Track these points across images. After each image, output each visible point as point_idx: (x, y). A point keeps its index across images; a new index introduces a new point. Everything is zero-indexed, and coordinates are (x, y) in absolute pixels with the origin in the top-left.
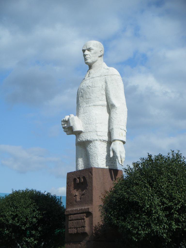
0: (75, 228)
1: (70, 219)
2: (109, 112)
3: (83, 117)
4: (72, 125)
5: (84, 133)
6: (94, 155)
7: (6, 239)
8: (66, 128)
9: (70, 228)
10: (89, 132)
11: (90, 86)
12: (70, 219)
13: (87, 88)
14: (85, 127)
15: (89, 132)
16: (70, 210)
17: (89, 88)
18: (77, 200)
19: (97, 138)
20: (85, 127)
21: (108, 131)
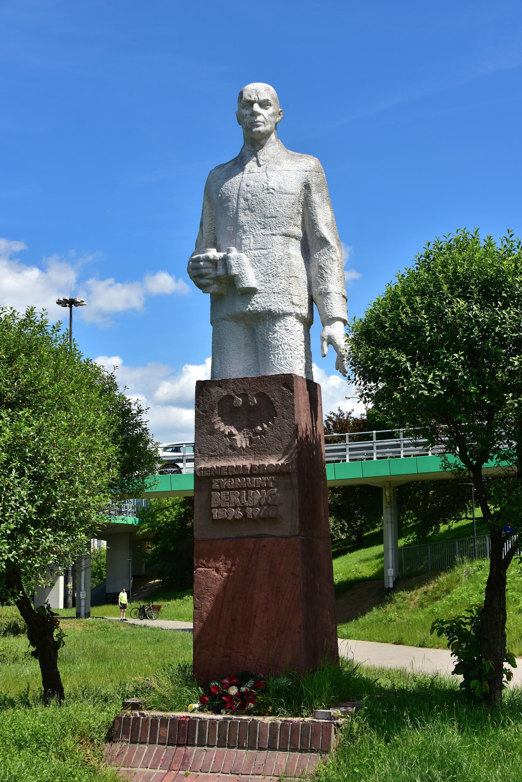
0: (235, 508)
1: (216, 486)
2: (307, 252)
3: (255, 257)
4: (235, 271)
5: (259, 293)
6: (283, 346)
7: (489, 505)
8: (209, 276)
9: (219, 507)
10: (274, 293)
11: (272, 189)
12: (216, 486)
13: (266, 191)
14: (262, 282)
15: (273, 295)
16: (267, 464)
17: (272, 194)
18: (239, 446)
19: (289, 308)
20: (262, 282)
21: (307, 296)
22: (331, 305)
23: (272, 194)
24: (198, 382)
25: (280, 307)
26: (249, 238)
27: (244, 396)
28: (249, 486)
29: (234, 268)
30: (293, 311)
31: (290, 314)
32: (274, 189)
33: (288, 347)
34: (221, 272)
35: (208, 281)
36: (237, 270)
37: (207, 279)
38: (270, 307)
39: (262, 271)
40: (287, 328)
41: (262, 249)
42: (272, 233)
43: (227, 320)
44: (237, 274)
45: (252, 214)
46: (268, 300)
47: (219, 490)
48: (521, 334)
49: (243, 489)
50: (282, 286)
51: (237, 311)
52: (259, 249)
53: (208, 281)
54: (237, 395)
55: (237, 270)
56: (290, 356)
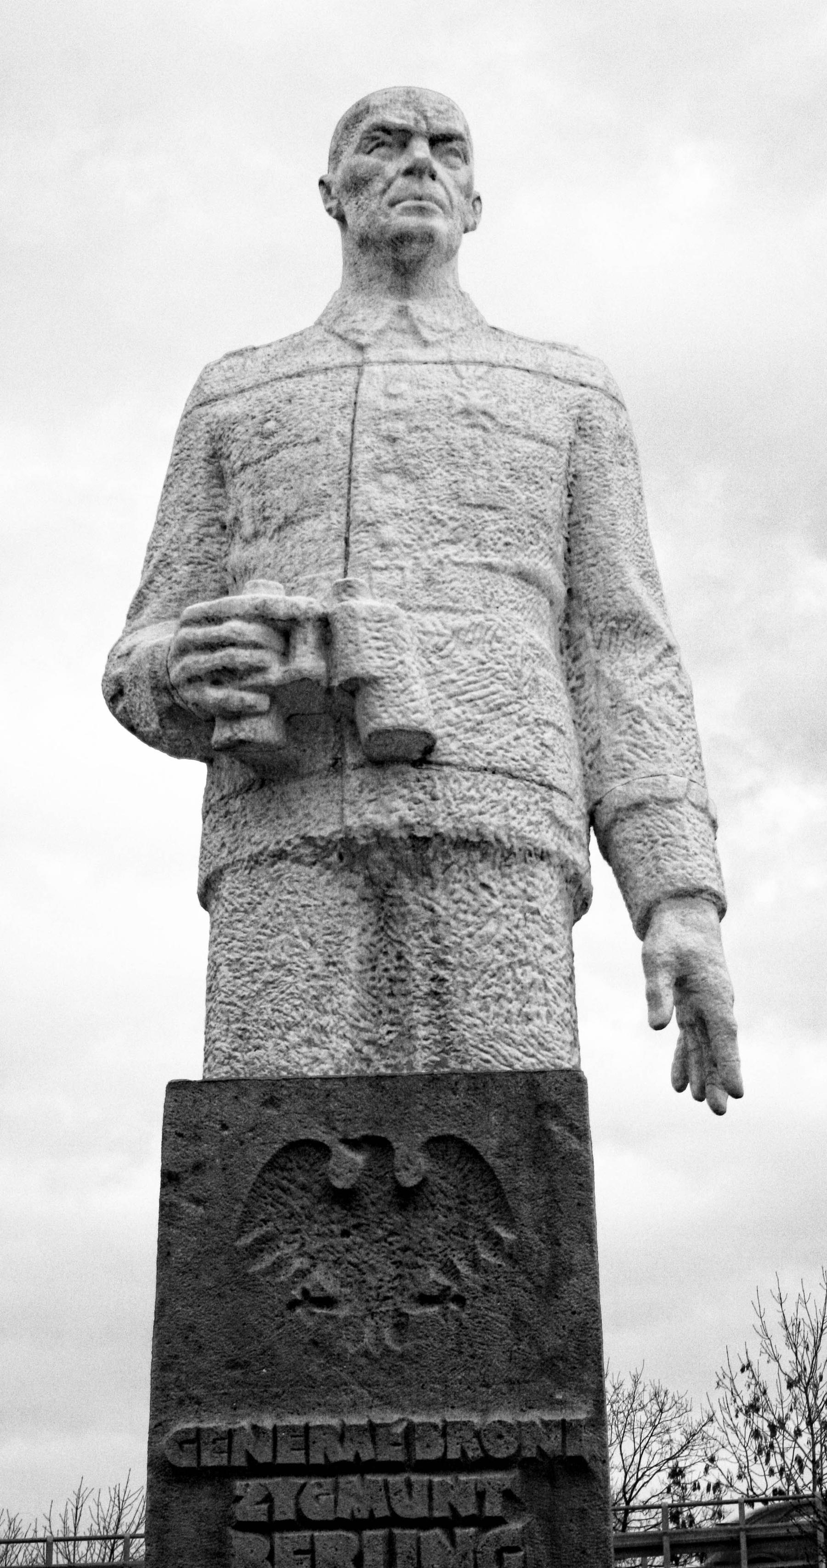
3: (424, 633)
6: (519, 971)
11: (484, 413)
17: (485, 429)
22: (683, 842)
23: (485, 429)
24: (176, 1088)
25: (514, 823)
26: (402, 569)
27: (377, 1146)
28: (399, 1511)
29: (367, 652)
30: (553, 847)
31: (543, 856)
32: (492, 418)
33: (535, 974)
34: (307, 660)
35: (250, 698)
36: (378, 662)
37: (255, 689)
38: (478, 818)
39: (452, 689)
40: (533, 904)
41: (452, 610)
42: (484, 560)
43: (298, 860)
44: (378, 674)
45: (411, 487)
46: (473, 792)
47: (267, 1528)
48: (823, 1567)
49: (373, 1522)
50: (522, 751)
51: (349, 822)
52: (436, 609)
53: (250, 698)
54: (345, 1141)
55: (378, 662)
56: (543, 1011)
